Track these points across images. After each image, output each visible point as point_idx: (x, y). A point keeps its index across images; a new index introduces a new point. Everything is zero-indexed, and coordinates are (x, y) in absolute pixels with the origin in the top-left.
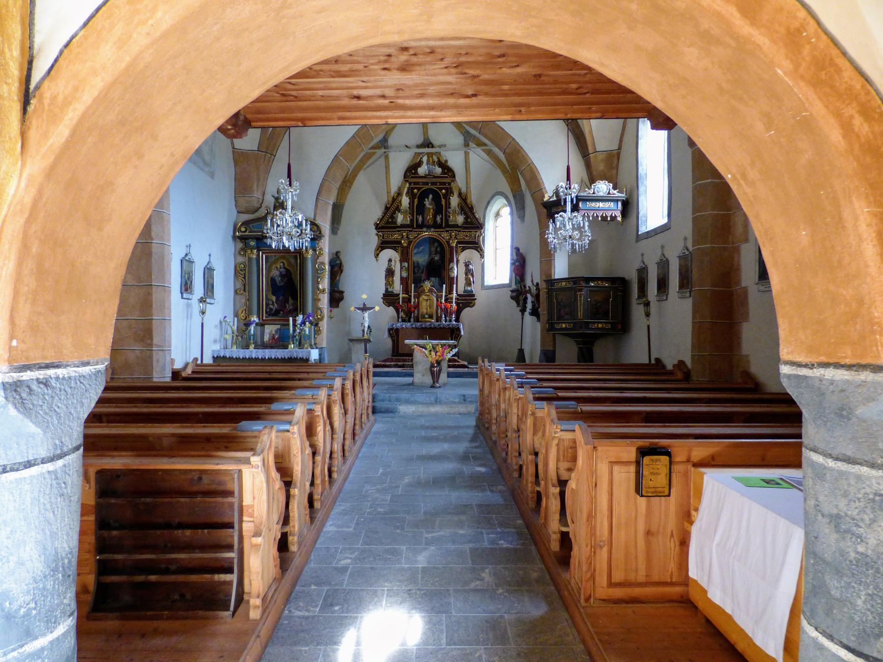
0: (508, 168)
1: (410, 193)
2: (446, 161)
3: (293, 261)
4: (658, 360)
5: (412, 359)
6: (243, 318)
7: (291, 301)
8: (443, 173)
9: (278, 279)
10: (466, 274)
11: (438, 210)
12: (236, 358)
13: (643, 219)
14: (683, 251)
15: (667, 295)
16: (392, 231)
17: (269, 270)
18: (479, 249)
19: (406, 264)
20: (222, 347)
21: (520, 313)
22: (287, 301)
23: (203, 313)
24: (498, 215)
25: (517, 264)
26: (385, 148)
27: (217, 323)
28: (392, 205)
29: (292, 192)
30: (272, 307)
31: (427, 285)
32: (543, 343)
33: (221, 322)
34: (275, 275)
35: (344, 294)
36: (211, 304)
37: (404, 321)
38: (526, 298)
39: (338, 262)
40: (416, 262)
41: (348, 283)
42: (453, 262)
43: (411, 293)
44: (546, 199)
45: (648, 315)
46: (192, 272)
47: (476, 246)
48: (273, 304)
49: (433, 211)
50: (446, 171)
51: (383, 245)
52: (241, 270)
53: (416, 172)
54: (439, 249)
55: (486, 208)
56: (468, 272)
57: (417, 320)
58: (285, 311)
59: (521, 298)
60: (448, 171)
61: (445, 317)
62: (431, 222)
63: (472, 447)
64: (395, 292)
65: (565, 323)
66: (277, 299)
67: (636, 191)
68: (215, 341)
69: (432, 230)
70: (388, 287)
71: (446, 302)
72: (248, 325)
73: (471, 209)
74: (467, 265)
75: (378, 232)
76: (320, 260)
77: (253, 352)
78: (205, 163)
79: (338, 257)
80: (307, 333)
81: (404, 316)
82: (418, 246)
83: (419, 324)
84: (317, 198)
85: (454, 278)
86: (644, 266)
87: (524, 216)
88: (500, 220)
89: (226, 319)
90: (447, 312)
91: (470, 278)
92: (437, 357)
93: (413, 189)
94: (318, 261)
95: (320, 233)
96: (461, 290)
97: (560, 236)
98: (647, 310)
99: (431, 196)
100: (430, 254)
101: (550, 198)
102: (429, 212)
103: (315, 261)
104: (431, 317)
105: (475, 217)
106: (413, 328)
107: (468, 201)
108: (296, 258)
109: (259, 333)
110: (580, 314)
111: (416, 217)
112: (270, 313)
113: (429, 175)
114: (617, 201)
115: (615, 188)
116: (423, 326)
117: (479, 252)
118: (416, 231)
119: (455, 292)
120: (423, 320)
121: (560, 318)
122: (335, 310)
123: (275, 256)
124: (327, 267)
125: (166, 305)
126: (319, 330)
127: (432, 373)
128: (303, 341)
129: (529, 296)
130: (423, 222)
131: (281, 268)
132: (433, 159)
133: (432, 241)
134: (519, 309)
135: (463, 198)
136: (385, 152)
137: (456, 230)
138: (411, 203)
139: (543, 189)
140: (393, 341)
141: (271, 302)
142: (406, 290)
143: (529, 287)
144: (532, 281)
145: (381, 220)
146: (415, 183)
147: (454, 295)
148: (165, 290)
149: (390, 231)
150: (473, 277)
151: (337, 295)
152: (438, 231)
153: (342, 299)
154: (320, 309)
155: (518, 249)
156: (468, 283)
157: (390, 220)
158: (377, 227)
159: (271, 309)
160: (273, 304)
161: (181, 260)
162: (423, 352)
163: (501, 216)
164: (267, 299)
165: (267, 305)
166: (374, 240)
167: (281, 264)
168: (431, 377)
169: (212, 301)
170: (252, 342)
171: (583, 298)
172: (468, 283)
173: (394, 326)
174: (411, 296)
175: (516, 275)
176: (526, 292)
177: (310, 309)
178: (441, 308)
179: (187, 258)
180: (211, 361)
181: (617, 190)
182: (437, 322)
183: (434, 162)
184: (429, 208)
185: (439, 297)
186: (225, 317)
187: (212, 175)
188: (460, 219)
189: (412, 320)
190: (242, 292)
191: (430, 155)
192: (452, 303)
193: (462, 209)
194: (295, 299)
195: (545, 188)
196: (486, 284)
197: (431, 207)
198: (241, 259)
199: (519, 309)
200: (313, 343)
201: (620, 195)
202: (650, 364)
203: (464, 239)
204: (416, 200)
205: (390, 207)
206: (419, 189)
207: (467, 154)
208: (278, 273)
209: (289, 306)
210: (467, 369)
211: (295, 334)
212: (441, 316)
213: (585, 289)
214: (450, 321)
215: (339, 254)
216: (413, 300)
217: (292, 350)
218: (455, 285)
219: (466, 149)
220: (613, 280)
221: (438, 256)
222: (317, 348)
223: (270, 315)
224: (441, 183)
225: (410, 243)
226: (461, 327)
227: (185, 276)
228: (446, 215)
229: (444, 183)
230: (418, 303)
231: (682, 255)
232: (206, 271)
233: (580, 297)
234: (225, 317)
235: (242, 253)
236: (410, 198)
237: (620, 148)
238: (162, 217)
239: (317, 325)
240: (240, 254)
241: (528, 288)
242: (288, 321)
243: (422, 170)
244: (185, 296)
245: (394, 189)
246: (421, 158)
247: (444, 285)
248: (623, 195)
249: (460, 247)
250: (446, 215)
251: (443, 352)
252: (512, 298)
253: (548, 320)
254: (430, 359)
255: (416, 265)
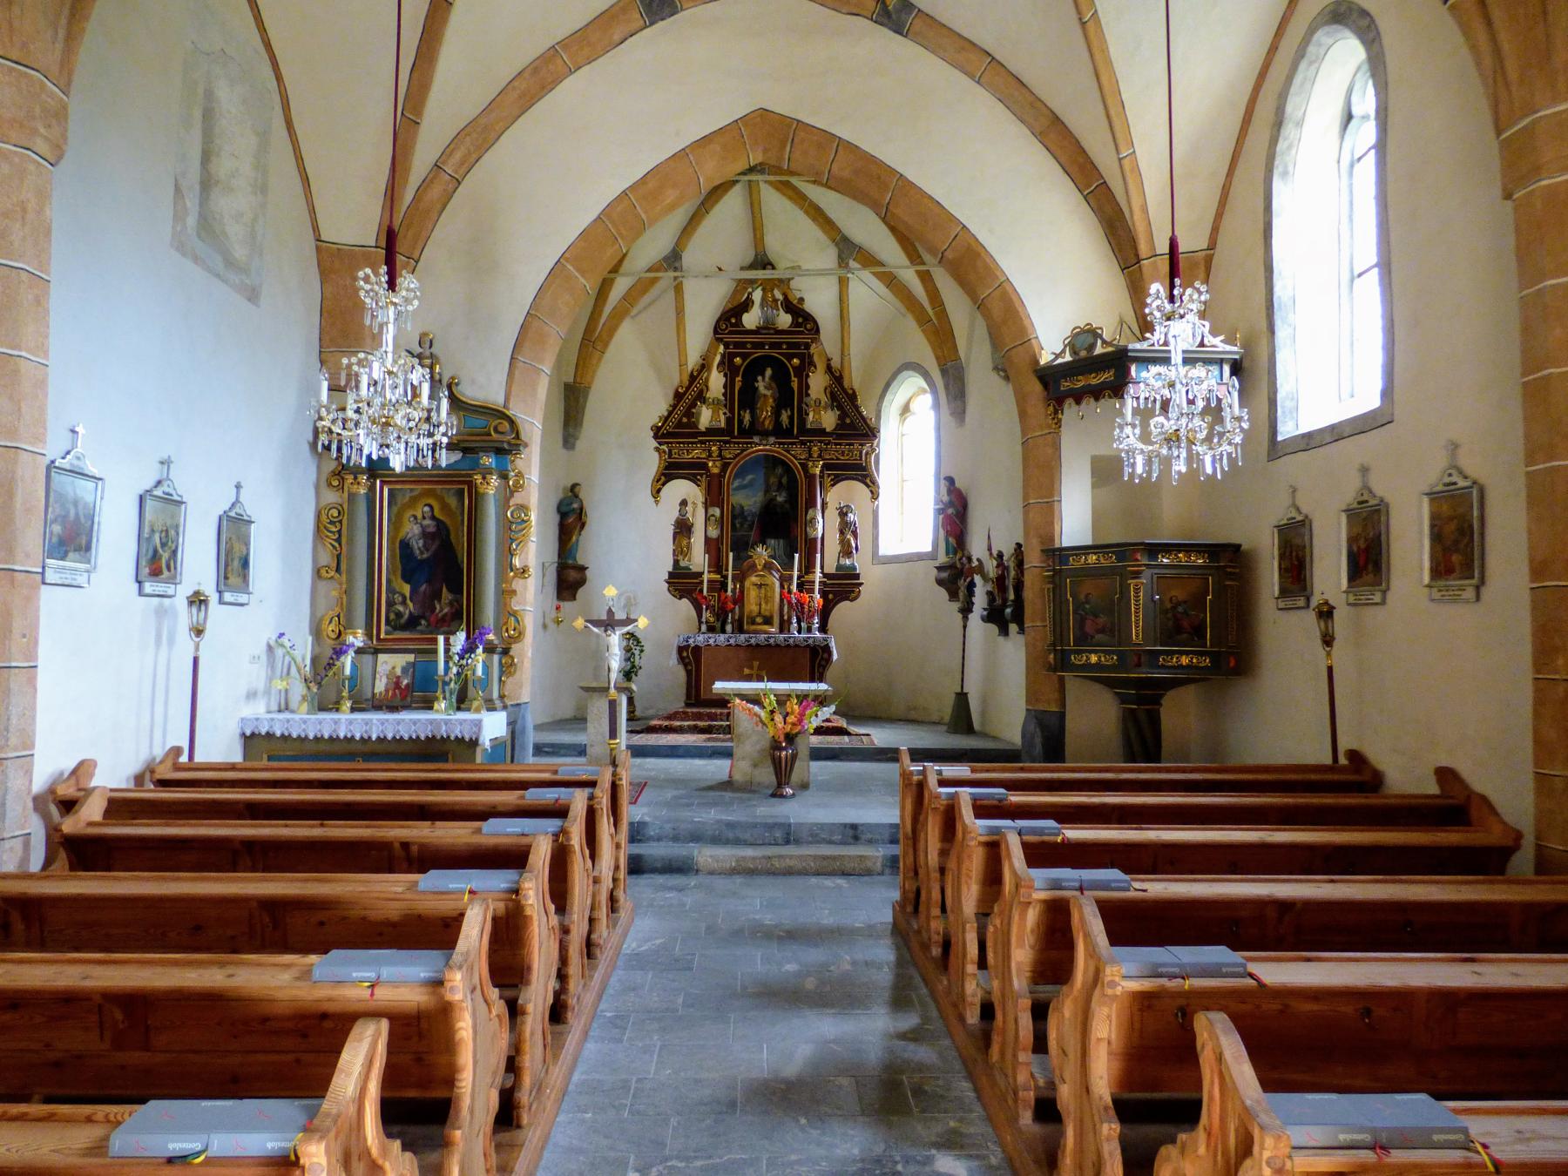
0: (931, 312)
1: (727, 365)
2: (801, 300)
3: (453, 502)
4: (1356, 757)
5: (729, 714)
6: (334, 636)
7: (446, 595)
8: (795, 324)
9: (417, 545)
10: (842, 532)
11: (785, 398)
12: (299, 737)
13: (1289, 404)
14: (1447, 480)
15: (1384, 592)
16: (688, 443)
17: (396, 523)
18: (868, 481)
19: (717, 512)
20: (275, 708)
21: (960, 616)
22: (438, 596)
23: (199, 632)
24: (906, 410)
25: (950, 511)
26: (676, 269)
27: (261, 649)
28: (688, 388)
29: (395, 304)
30: (401, 608)
31: (761, 554)
32: (1032, 695)
33: (270, 648)
34: (410, 535)
35: (587, 572)
36: (242, 605)
37: (711, 629)
38: (972, 585)
39: (575, 506)
40: (737, 507)
41: (593, 548)
42: (815, 505)
43: (727, 570)
44: (1042, 362)
45: (1328, 640)
46: (177, 526)
47: (863, 473)
48: (404, 603)
49: (775, 401)
50: (800, 320)
51: (670, 471)
52: (331, 523)
53: (739, 323)
54: (784, 480)
55: (1274, 141)
56: (846, 527)
57: (739, 629)
58: (433, 619)
59: (962, 584)
60: (804, 321)
61: (799, 622)
62: (768, 425)
63: (903, 1036)
64: (694, 569)
65: (1095, 652)
66: (413, 592)
67: (1264, 342)
68: (251, 695)
69: (772, 440)
70: (680, 558)
71: (801, 591)
72: (339, 652)
73: (853, 397)
74: (843, 514)
75: (660, 444)
76: (517, 499)
77: (347, 723)
78: (230, 263)
79: (576, 496)
80: (479, 672)
81: (712, 619)
82: (740, 474)
83: (742, 637)
84: (512, 358)
85: (815, 539)
86: (1299, 518)
87: (964, 412)
88: (910, 419)
89: (284, 640)
90: (803, 613)
91: (849, 540)
92: (788, 728)
93: (732, 356)
94: (511, 503)
95: (518, 437)
96: (831, 568)
97: (1155, 431)
98: (1327, 628)
99: (769, 372)
100: (767, 491)
101: (1057, 356)
102: (765, 402)
103: (504, 503)
104: (768, 621)
105: (860, 414)
106: (730, 645)
107: (846, 384)
108: (460, 493)
109: (367, 672)
110: (1136, 634)
111: (739, 414)
112: (396, 624)
113: (767, 328)
114: (1221, 362)
115: (1214, 333)
116: (753, 641)
117: (868, 486)
118: (738, 443)
119: (818, 569)
120: (753, 627)
121: (1083, 639)
122: (566, 605)
123: (412, 490)
124: (533, 518)
125: (18, 625)
126: (512, 664)
127: (776, 763)
128: (471, 691)
129: (978, 579)
130: (752, 423)
131: (424, 518)
132: (773, 296)
133: (772, 462)
134: (956, 606)
135: (836, 378)
136: (676, 278)
137: (820, 442)
138: (729, 386)
139: (1033, 341)
140: (689, 673)
141: (398, 598)
142: (717, 565)
143: (978, 560)
144: (990, 549)
145: (666, 419)
146: (737, 345)
147: (818, 576)
148: (12, 582)
149: (683, 443)
150: (856, 537)
151: (572, 575)
152: (784, 444)
153: (582, 582)
154: (514, 614)
155: (950, 480)
156: (847, 551)
157: (685, 420)
158: (658, 433)
159: (399, 615)
160: (404, 603)
161: (141, 499)
162: (756, 715)
163: (914, 414)
164: (390, 590)
165: (390, 604)
166: (652, 463)
167: (427, 509)
168: (771, 769)
169: (243, 598)
170: (345, 694)
171: (1141, 595)
172: (847, 551)
173: (691, 641)
174: (726, 577)
175: (948, 534)
176: (972, 571)
177: (489, 615)
178: (790, 603)
179: (158, 492)
180: (233, 753)
181: (1222, 337)
182: (781, 631)
183: (775, 301)
184: (765, 396)
185: (785, 580)
186: (282, 635)
187: (253, 295)
188: (829, 420)
189: (729, 628)
190: (332, 573)
191: (768, 286)
192: (812, 591)
193: (833, 397)
194: (456, 589)
195: (1037, 338)
196: (882, 552)
197: (769, 393)
198: (331, 497)
199: (956, 606)
200: (495, 695)
201: (1228, 348)
202: (1334, 767)
203: (838, 459)
204: (739, 378)
205: (685, 393)
206: (744, 356)
207: (843, 283)
208: (417, 530)
209: (442, 608)
210: (846, 738)
211: (447, 679)
212: (790, 618)
213: (1147, 573)
214: (809, 630)
215: (576, 490)
216: (730, 586)
217: (442, 718)
218: (818, 556)
219: (842, 272)
220: (1215, 551)
221: (784, 494)
222: (505, 707)
223: (395, 628)
224: (791, 345)
225: (725, 467)
226: (833, 644)
227: (149, 539)
228: (800, 409)
229: (796, 345)
230: (742, 592)
231: (1440, 488)
232: (225, 523)
233: (1137, 591)
234: (282, 635)
235: (335, 483)
236: (725, 375)
237: (1212, 245)
238: (16, 372)
239: (506, 652)
240: (330, 485)
241: (975, 563)
242: (435, 641)
243: (751, 320)
244: (149, 587)
245: (693, 360)
246: (750, 294)
247: (797, 556)
248: (1235, 349)
249: (829, 475)
250: (800, 409)
251: (802, 715)
252: (940, 582)
253: (1054, 644)
254: (771, 731)
255: (737, 511)
